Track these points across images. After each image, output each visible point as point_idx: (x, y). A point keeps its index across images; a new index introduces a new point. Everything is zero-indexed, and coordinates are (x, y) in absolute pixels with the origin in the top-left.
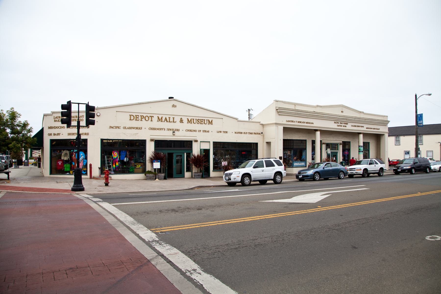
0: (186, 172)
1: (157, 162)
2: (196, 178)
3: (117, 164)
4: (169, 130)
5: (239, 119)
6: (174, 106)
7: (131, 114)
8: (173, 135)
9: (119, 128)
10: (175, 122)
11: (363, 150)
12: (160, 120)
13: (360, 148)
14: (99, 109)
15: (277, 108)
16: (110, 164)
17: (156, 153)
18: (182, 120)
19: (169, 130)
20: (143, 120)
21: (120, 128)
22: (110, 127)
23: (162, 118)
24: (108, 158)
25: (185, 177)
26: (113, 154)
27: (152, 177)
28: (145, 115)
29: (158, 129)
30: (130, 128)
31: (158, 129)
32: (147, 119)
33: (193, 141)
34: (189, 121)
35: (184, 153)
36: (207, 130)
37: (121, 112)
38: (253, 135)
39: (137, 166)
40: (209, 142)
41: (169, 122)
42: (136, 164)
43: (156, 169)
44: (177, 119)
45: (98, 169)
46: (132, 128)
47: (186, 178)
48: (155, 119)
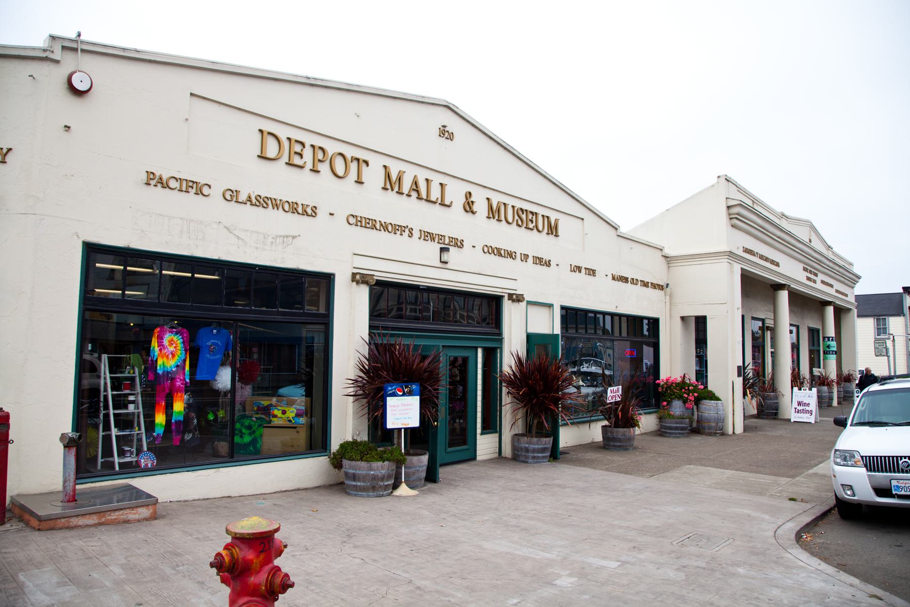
0: (482, 434)
1: (404, 395)
2: (531, 461)
3: (179, 407)
4: (428, 236)
5: (623, 230)
6: (445, 133)
7: (268, 127)
8: (440, 265)
9: (199, 192)
10: (449, 206)
11: (837, 348)
12: (392, 183)
13: (829, 343)
14: (83, 51)
15: (731, 203)
16: (131, 407)
17: (376, 345)
18: (472, 202)
19: (428, 236)
20: (324, 168)
21: (206, 190)
22: (149, 179)
23: (400, 179)
24: (115, 366)
25: (478, 458)
26: (154, 344)
27: (382, 479)
28: (332, 148)
29: (385, 227)
30: (261, 202)
31: (385, 227)
32: (340, 168)
33: (506, 296)
34: (494, 212)
35: (476, 348)
36: (546, 257)
37: (216, 106)
38: (650, 290)
39: (276, 412)
40: (550, 306)
41: (428, 200)
42: (265, 403)
43: (400, 429)
44: (455, 194)
45: (61, 446)
46: (269, 202)
47: (479, 461)
48: (374, 175)
